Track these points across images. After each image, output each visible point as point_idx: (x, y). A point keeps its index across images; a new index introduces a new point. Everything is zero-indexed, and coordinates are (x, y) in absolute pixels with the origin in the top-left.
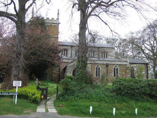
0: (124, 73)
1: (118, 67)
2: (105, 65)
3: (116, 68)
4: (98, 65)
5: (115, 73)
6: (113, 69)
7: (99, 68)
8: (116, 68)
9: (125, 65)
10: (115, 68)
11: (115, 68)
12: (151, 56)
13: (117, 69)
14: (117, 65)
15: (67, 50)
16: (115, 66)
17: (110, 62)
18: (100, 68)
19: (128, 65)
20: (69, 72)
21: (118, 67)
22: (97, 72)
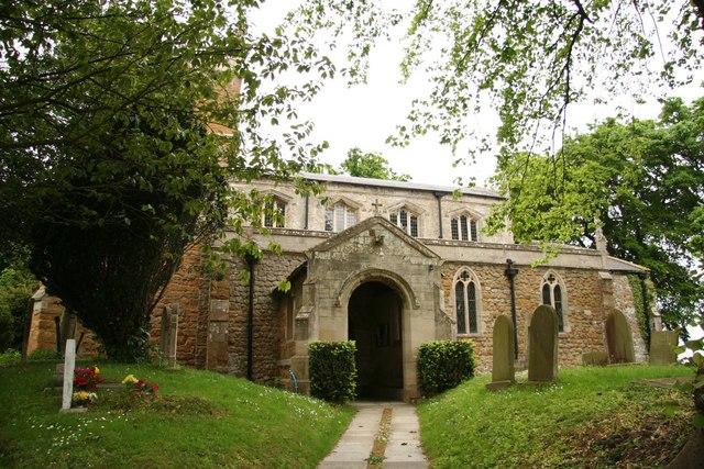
0: (588, 312)
1: (560, 280)
2: (502, 272)
3: (552, 286)
4: (461, 269)
5: (470, 319)
6: (541, 290)
7: (471, 285)
8: (552, 286)
9: (593, 270)
10: (546, 288)
11: (546, 288)
12: (659, 124)
13: (557, 289)
14: (470, 270)
15: (282, 204)
16: (546, 275)
17: (491, 252)
18: (564, 290)
19: (601, 270)
20: (328, 303)
21: (560, 280)
22: (460, 302)
